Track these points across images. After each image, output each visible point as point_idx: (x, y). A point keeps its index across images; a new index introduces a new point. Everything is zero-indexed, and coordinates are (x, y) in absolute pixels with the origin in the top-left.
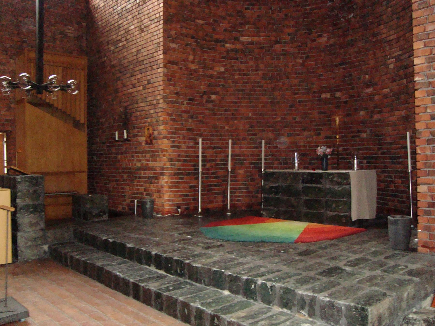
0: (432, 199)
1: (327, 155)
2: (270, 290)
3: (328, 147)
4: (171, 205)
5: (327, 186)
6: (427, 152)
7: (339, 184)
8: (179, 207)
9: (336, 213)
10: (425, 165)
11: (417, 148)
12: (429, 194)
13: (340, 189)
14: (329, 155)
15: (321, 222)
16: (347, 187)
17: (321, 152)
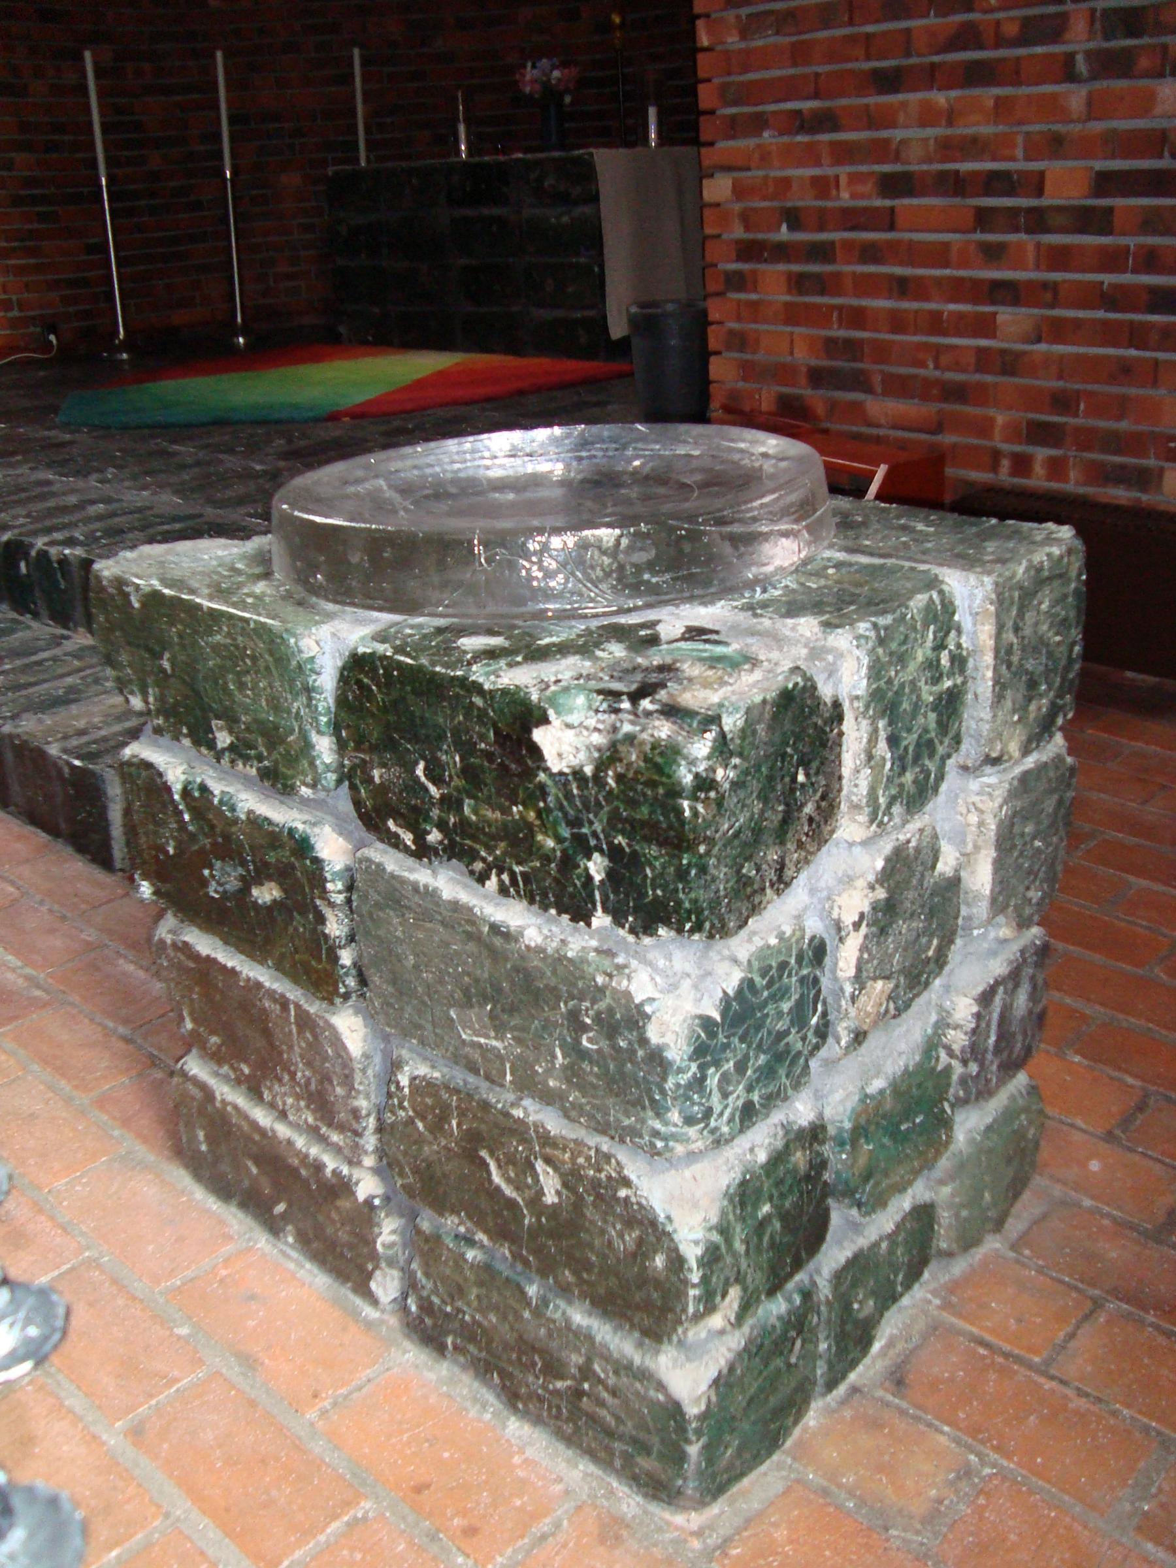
0: (747, 229)
1: (561, 96)
2: (59, 575)
3: (564, 65)
4: (14, 323)
5: (527, 212)
6: (730, 40)
7: (564, 199)
8: (53, 329)
9: (560, 313)
10: (729, 95)
11: (700, 24)
12: (737, 207)
13: (565, 219)
14: (567, 91)
15: (513, 348)
16: (587, 210)
17: (534, 81)
